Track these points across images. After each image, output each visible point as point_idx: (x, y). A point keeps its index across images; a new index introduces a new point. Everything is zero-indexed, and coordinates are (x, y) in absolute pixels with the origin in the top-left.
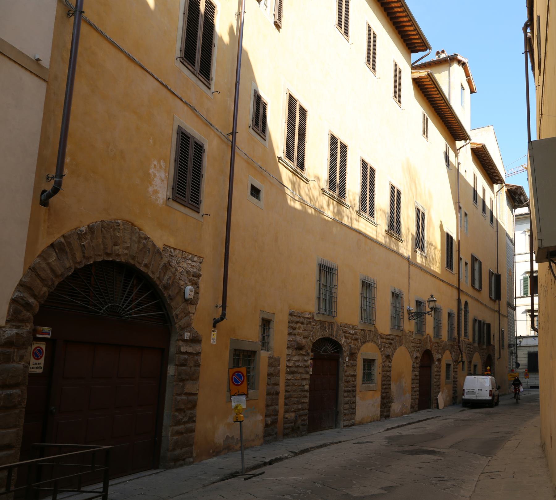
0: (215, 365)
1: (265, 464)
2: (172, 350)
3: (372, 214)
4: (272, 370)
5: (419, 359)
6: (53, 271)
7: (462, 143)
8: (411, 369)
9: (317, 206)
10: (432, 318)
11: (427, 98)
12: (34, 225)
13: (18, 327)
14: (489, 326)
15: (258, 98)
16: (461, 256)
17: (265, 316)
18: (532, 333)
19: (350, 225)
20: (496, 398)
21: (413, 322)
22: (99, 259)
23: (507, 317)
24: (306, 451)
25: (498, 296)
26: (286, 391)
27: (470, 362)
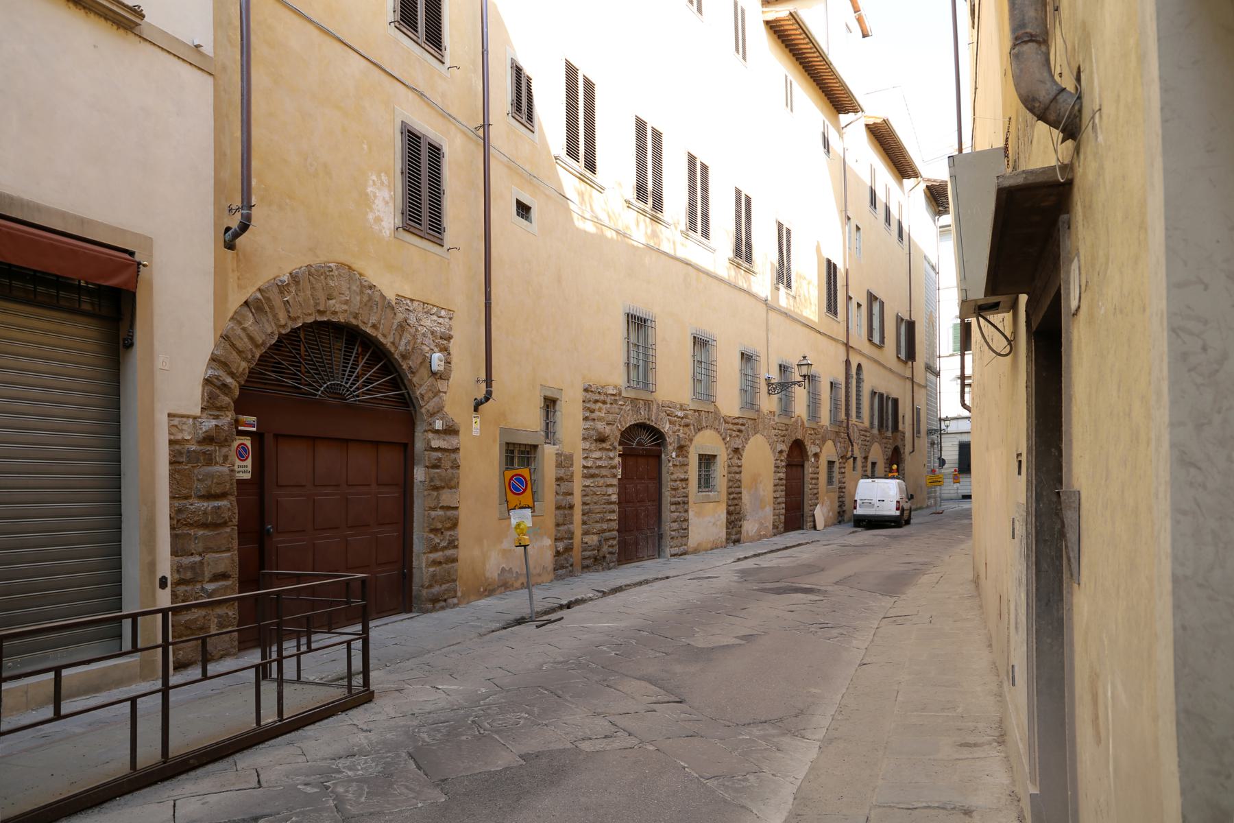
0: (480, 466)
1: (561, 607)
2: (419, 445)
3: (706, 234)
4: (562, 472)
5: (785, 454)
6: (251, 339)
7: (850, 117)
8: (773, 469)
9: (620, 227)
10: (805, 391)
11: (791, 51)
12: (220, 273)
13: (216, 417)
14: (896, 401)
15: (518, 71)
16: (850, 294)
17: (549, 394)
18: (966, 413)
19: (672, 253)
20: (906, 513)
21: (775, 398)
22: (310, 320)
23: (925, 387)
24: (619, 589)
25: (911, 355)
26: (584, 504)
27: (866, 458)
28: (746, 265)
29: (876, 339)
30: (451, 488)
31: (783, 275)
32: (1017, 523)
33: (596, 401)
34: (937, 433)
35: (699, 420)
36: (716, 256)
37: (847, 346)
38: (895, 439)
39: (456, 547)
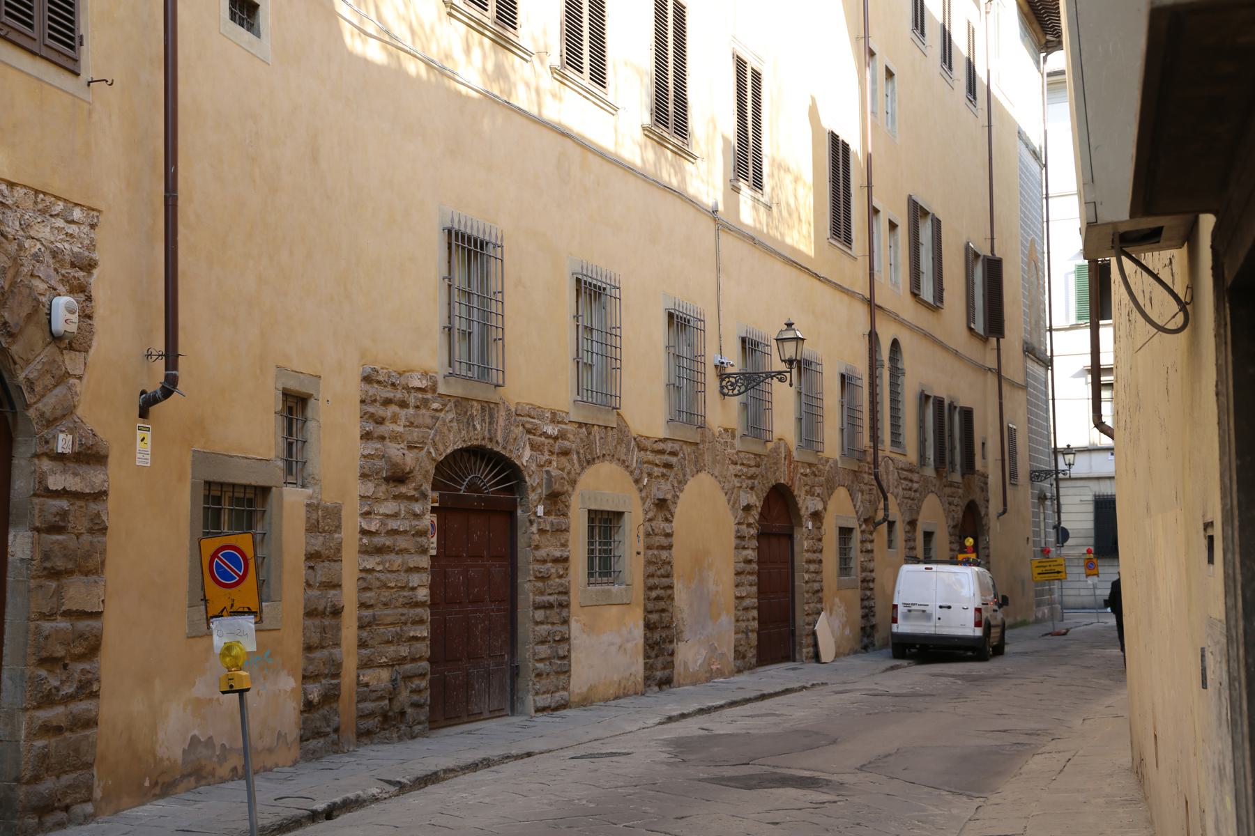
0: (149, 532)
2: (21, 485)
3: (599, 75)
4: (318, 543)
8: (733, 542)
9: (434, 53)
10: (792, 391)
14: (967, 414)
16: (876, 203)
17: (293, 385)
18: (1106, 441)
19: (534, 110)
20: (995, 632)
21: (735, 402)
23: (1024, 387)
24: (431, 779)
25: (995, 325)
26: (363, 605)
27: (912, 523)
28: (677, 141)
29: (927, 293)
30: (87, 573)
31: (747, 162)
32: (1209, 656)
33: (387, 402)
34: (1050, 475)
35: (589, 446)
36: (616, 120)
37: (871, 303)
38: (968, 488)
39: (737, 598)
